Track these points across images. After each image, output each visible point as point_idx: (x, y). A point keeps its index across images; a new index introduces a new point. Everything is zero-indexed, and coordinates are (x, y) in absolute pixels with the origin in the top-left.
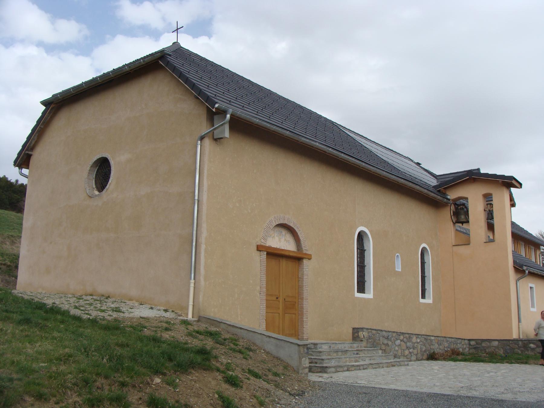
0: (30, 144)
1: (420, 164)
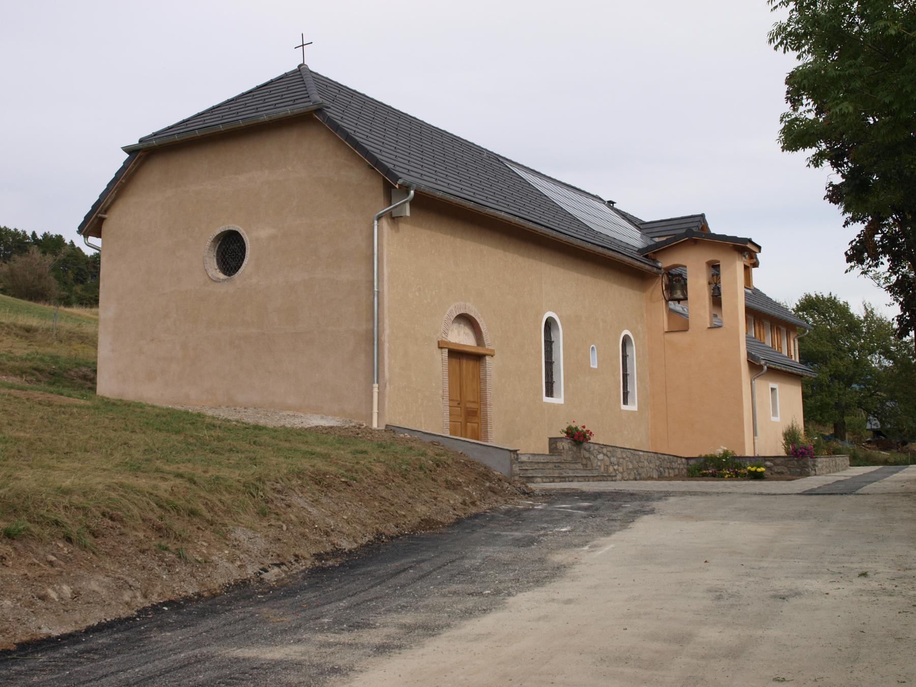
0: (104, 205)
1: (613, 203)
